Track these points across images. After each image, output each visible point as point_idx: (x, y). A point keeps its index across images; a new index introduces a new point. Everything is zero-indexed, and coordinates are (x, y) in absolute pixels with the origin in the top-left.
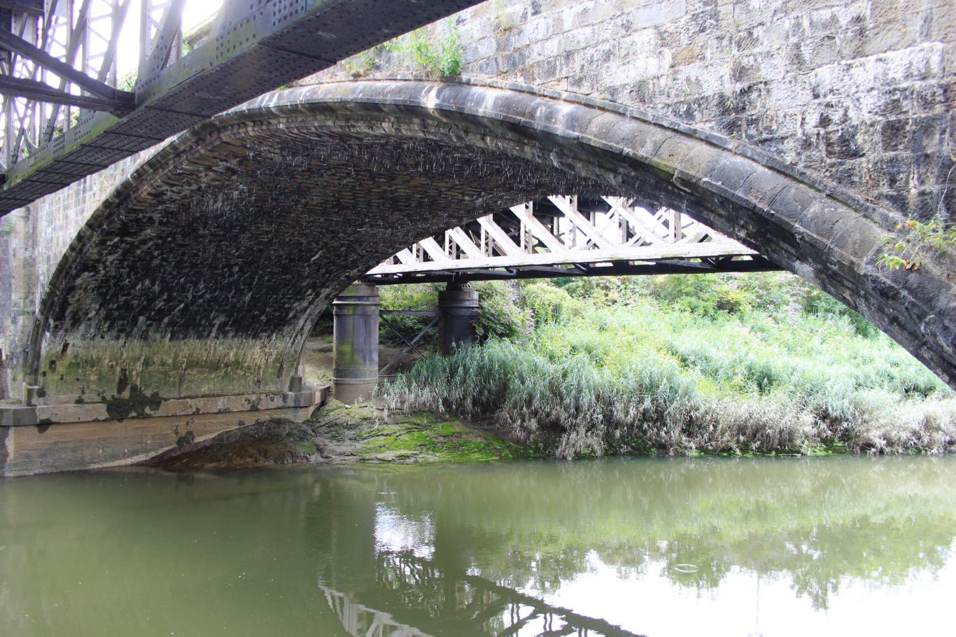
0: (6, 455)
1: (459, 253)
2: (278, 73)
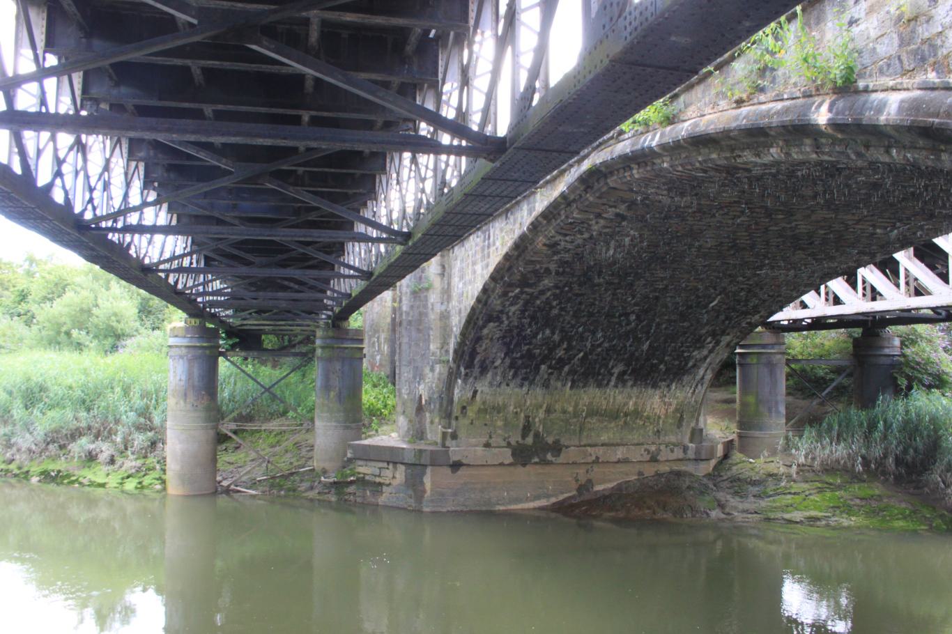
0: (424, 491)
1: (875, 294)
2: (637, 94)
